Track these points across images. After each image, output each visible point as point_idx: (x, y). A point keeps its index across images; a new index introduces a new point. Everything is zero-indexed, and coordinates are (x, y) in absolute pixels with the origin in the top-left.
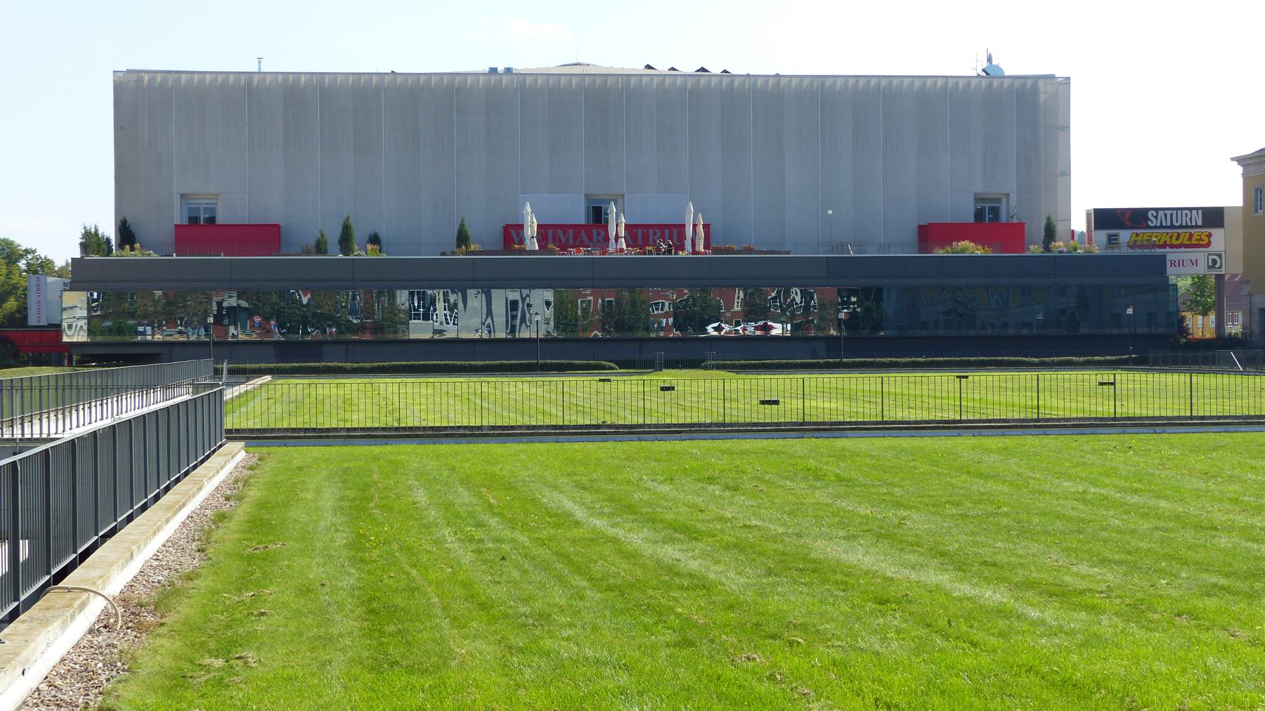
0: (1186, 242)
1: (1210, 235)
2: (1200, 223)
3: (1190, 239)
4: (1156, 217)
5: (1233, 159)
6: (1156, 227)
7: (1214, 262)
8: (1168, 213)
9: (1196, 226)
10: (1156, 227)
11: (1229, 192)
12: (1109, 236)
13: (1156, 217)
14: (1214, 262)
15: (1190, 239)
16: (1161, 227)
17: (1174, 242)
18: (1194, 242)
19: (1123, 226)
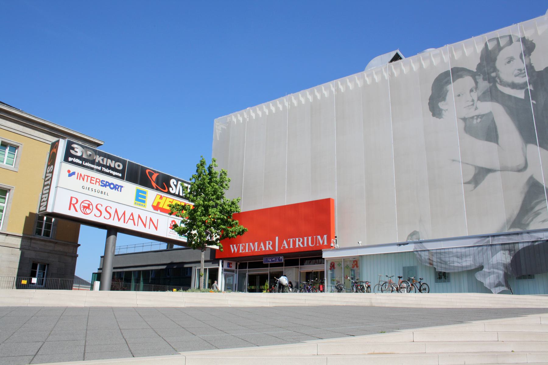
4: (176, 186)
6: (174, 194)
10: (174, 194)
12: (138, 191)
13: (176, 186)
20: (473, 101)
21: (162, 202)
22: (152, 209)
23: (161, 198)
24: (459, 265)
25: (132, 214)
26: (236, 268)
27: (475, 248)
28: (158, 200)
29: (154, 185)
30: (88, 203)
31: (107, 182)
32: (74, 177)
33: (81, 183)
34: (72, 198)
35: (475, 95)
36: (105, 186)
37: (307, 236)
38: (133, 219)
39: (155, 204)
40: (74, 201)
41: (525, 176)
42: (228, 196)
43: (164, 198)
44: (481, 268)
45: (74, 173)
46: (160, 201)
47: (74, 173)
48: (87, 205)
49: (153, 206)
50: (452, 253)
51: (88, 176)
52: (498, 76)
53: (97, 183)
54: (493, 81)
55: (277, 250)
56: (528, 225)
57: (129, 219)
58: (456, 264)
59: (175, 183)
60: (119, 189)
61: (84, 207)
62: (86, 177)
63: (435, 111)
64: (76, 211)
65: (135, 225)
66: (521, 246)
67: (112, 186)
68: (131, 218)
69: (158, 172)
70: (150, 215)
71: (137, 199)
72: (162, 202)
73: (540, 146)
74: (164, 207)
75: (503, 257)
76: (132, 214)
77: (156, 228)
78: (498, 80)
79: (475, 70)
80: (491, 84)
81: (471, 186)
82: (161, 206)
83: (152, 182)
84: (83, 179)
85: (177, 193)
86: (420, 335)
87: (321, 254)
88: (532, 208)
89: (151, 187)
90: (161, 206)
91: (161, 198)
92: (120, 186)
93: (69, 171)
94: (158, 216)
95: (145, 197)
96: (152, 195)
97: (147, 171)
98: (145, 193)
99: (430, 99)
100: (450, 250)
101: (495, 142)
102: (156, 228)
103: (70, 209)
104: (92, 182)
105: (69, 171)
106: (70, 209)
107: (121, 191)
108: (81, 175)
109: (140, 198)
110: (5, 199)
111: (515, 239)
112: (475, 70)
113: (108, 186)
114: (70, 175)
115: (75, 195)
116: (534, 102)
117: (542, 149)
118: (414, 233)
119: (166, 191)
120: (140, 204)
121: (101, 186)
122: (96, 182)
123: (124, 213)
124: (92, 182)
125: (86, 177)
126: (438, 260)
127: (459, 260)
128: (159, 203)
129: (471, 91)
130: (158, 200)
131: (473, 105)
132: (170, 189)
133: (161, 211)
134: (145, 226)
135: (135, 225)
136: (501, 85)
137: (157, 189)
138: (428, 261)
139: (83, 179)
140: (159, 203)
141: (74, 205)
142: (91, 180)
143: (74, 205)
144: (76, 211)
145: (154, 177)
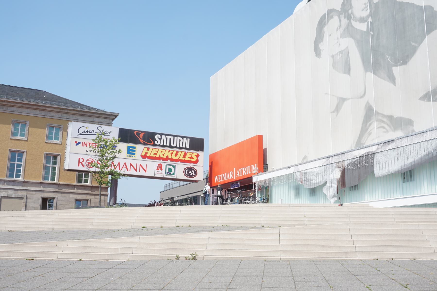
0: (182, 158)
1: (198, 156)
2: (188, 147)
3: (184, 156)
4: (160, 139)
5: (420, 99)
6: (159, 145)
7: (170, 170)
8: (169, 137)
9: (186, 148)
10: (159, 145)
11: (113, 122)
12: (129, 147)
13: (160, 139)
14: (170, 170)
15: (184, 156)
16: (163, 146)
17: (174, 157)
18: (187, 158)
19: (136, 141)
20: (338, 38)
21: (149, 152)
22: (141, 158)
23: (148, 149)
24: (315, 182)
25: (125, 164)
26: (225, 194)
27: (323, 167)
28: (145, 151)
29: (141, 141)
30: (91, 160)
32: (80, 145)
33: (85, 148)
34: (79, 159)
35: (339, 33)
37: (248, 166)
38: (126, 167)
39: (143, 154)
40: (81, 160)
41: (362, 103)
42: (395, 117)
43: (151, 150)
44: (325, 183)
45: (79, 143)
46: (147, 151)
47: (79, 143)
48: (90, 162)
49: (142, 156)
50: (311, 172)
51: (90, 143)
52: (352, 13)
54: (349, 17)
56: (365, 143)
57: (123, 167)
58: (314, 182)
59: (160, 137)
61: (89, 163)
62: (88, 144)
63: (317, 52)
64: (83, 166)
65: (128, 170)
66: (346, 163)
68: (125, 166)
69: (144, 132)
70: (139, 163)
71: (128, 153)
72: (149, 152)
73: (373, 73)
74: (151, 156)
75: (337, 174)
76: (125, 164)
77: (145, 171)
78: (352, 17)
79: (340, 10)
80: (348, 21)
81: (335, 114)
82: (148, 155)
83: (140, 139)
84: (87, 146)
85: (162, 144)
87: (252, 180)
88: (367, 129)
89: (140, 143)
90: (148, 155)
91: (148, 149)
93: (76, 142)
94: (144, 162)
95: (135, 151)
96: (140, 149)
97: (135, 132)
98: (135, 148)
99: (315, 42)
100: (309, 170)
101: (348, 74)
102: (145, 171)
103: (79, 166)
105: (76, 142)
106: (79, 166)
108: (84, 143)
109: (131, 152)
111: (343, 157)
112: (340, 10)
114: (77, 145)
115: (81, 156)
116: (372, 33)
117: (374, 75)
118: (305, 157)
119: (153, 143)
120: (131, 156)
123: (119, 164)
124: (93, 146)
125: (88, 144)
126: (305, 179)
127: (315, 178)
128: (146, 153)
129: (337, 29)
130: (145, 151)
131: (338, 42)
132: (156, 142)
133: (148, 159)
134: (136, 170)
135: (128, 170)
136: (354, 21)
137: (144, 144)
138: (300, 180)
139: (87, 146)
140: (146, 153)
141: (81, 163)
143: (81, 163)
144: (83, 166)
145: (141, 135)
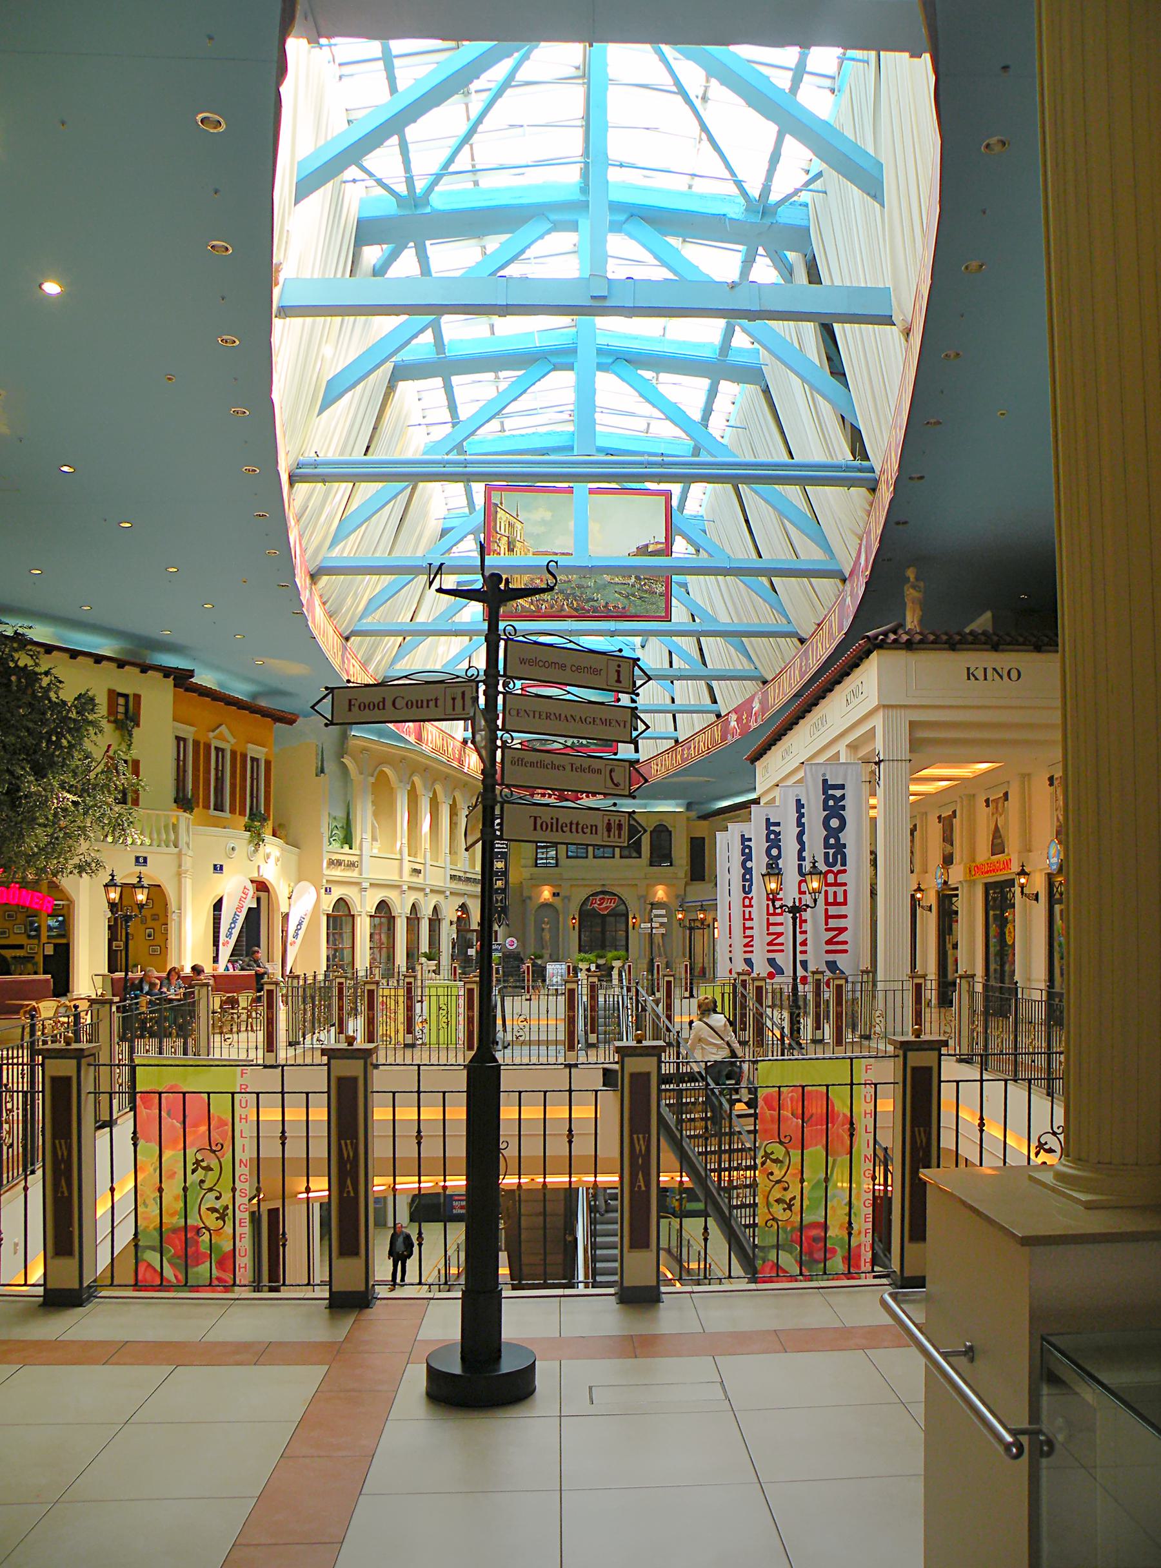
31: (827, 845)
36: (840, 848)
53: (841, 878)
55: (375, 1189)
60: (777, 829)
62: (833, 923)
67: (834, 823)
86: (489, 115)
92: (743, 843)
104: (840, 899)
107: (842, 787)
108: (770, 944)
110: (257, 1289)
113: (838, 839)
121: (844, 864)
122: (836, 884)
124: (840, 899)
125: (773, 929)
139: (842, 930)
142: (835, 903)
